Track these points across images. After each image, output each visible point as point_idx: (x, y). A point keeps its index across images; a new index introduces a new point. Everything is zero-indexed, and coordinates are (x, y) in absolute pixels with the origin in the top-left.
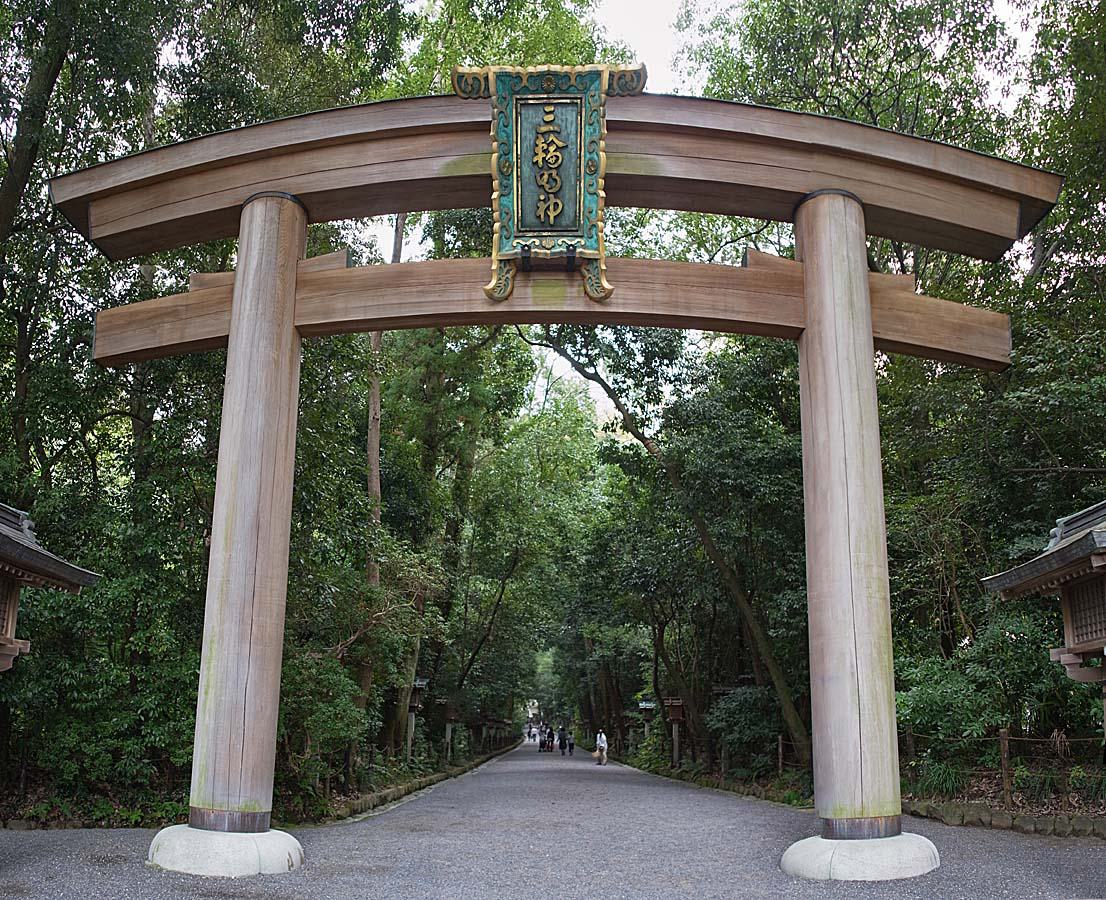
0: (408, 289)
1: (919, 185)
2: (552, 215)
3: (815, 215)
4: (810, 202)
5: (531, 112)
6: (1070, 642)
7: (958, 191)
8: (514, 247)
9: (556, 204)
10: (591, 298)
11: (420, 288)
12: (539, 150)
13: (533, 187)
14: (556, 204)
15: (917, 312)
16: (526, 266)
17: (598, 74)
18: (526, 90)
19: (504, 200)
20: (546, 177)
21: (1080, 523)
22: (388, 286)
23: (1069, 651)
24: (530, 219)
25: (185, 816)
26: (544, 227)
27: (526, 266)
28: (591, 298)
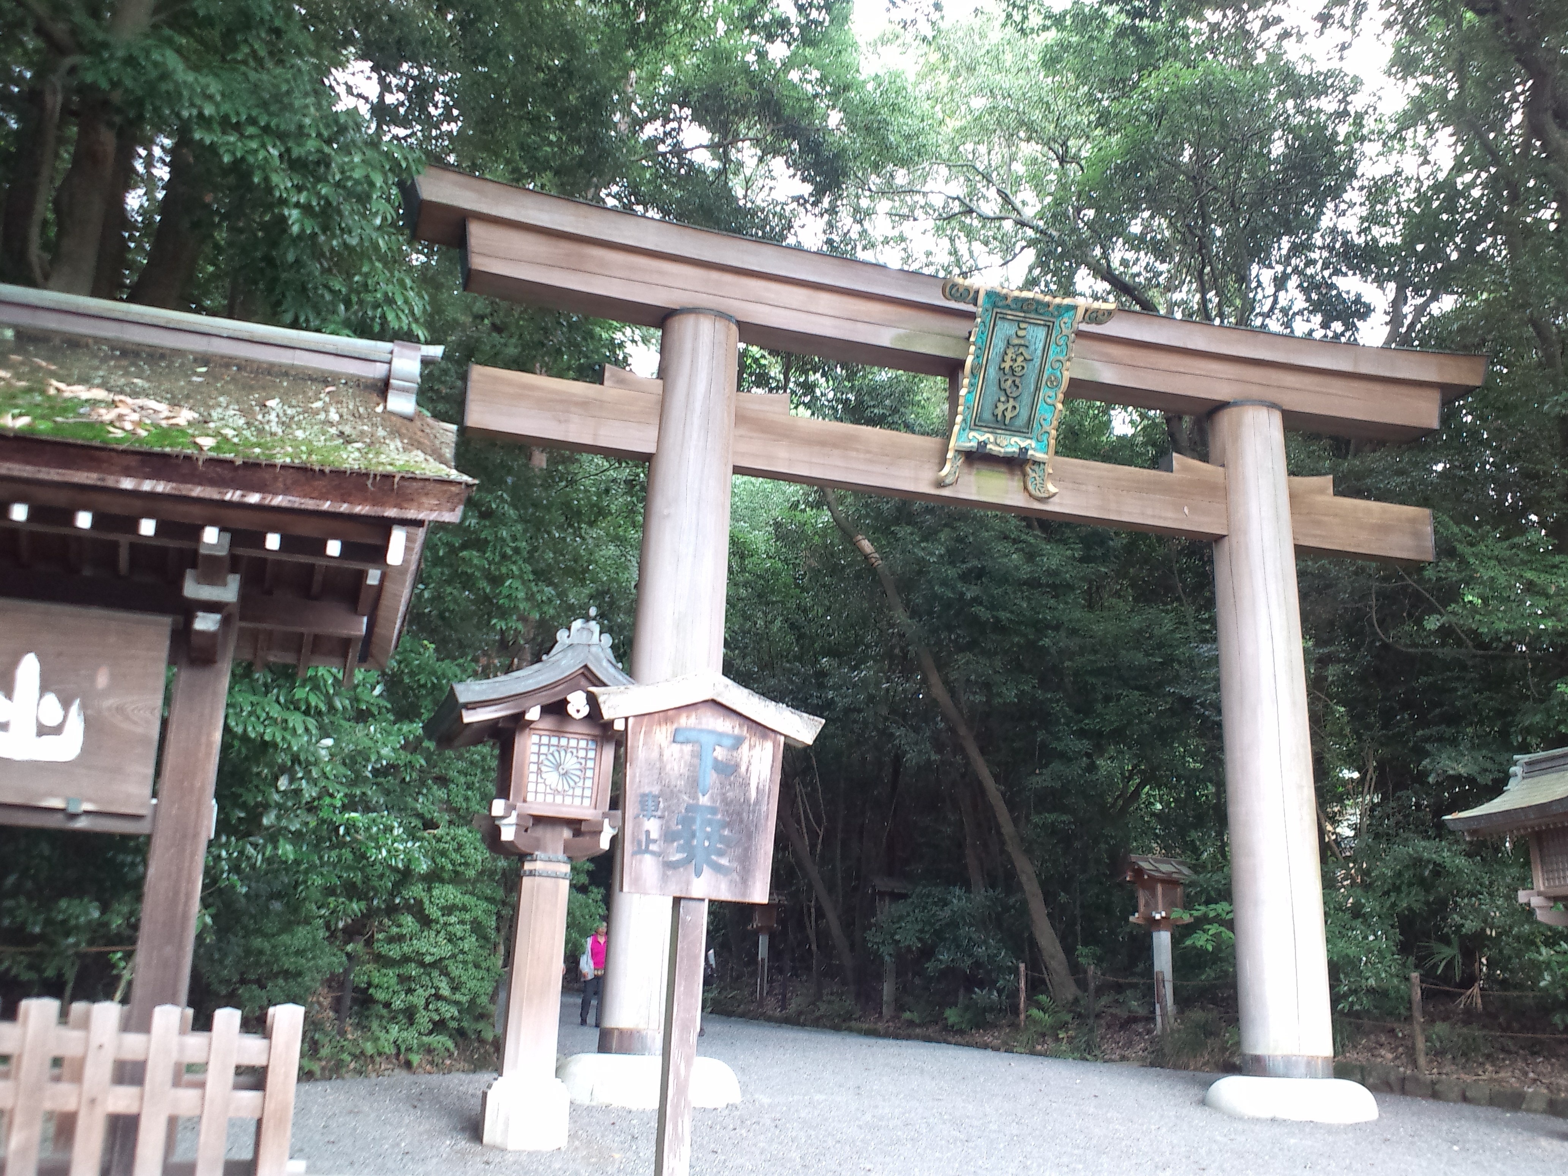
0: (854, 454)
1: (1337, 386)
2: (1009, 415)
3: (1239, 424)
4: (1234, 410)
5: (1006, 324)
6: (1540, 883)
7: (1378, 388)
8: (972, 439)
9: (1014, 407)
10: (1031, 495)
11: (868, 456)
12: (1008, 358)
13: (995, 388)
14: (1014, 407)
15: (1336, 515)
16: (977, 458)
17: (1075, 308)
18: (1008, 307)
19: (971, 397)
20: (1009, 382)
21: (1544, 766)
22: (835, 446)
23: (1539, 894)
24: (987, 415)
25: (1254, 1066)
26: (1000, 424)
27: (977, 458)
28: (1031, 495)
